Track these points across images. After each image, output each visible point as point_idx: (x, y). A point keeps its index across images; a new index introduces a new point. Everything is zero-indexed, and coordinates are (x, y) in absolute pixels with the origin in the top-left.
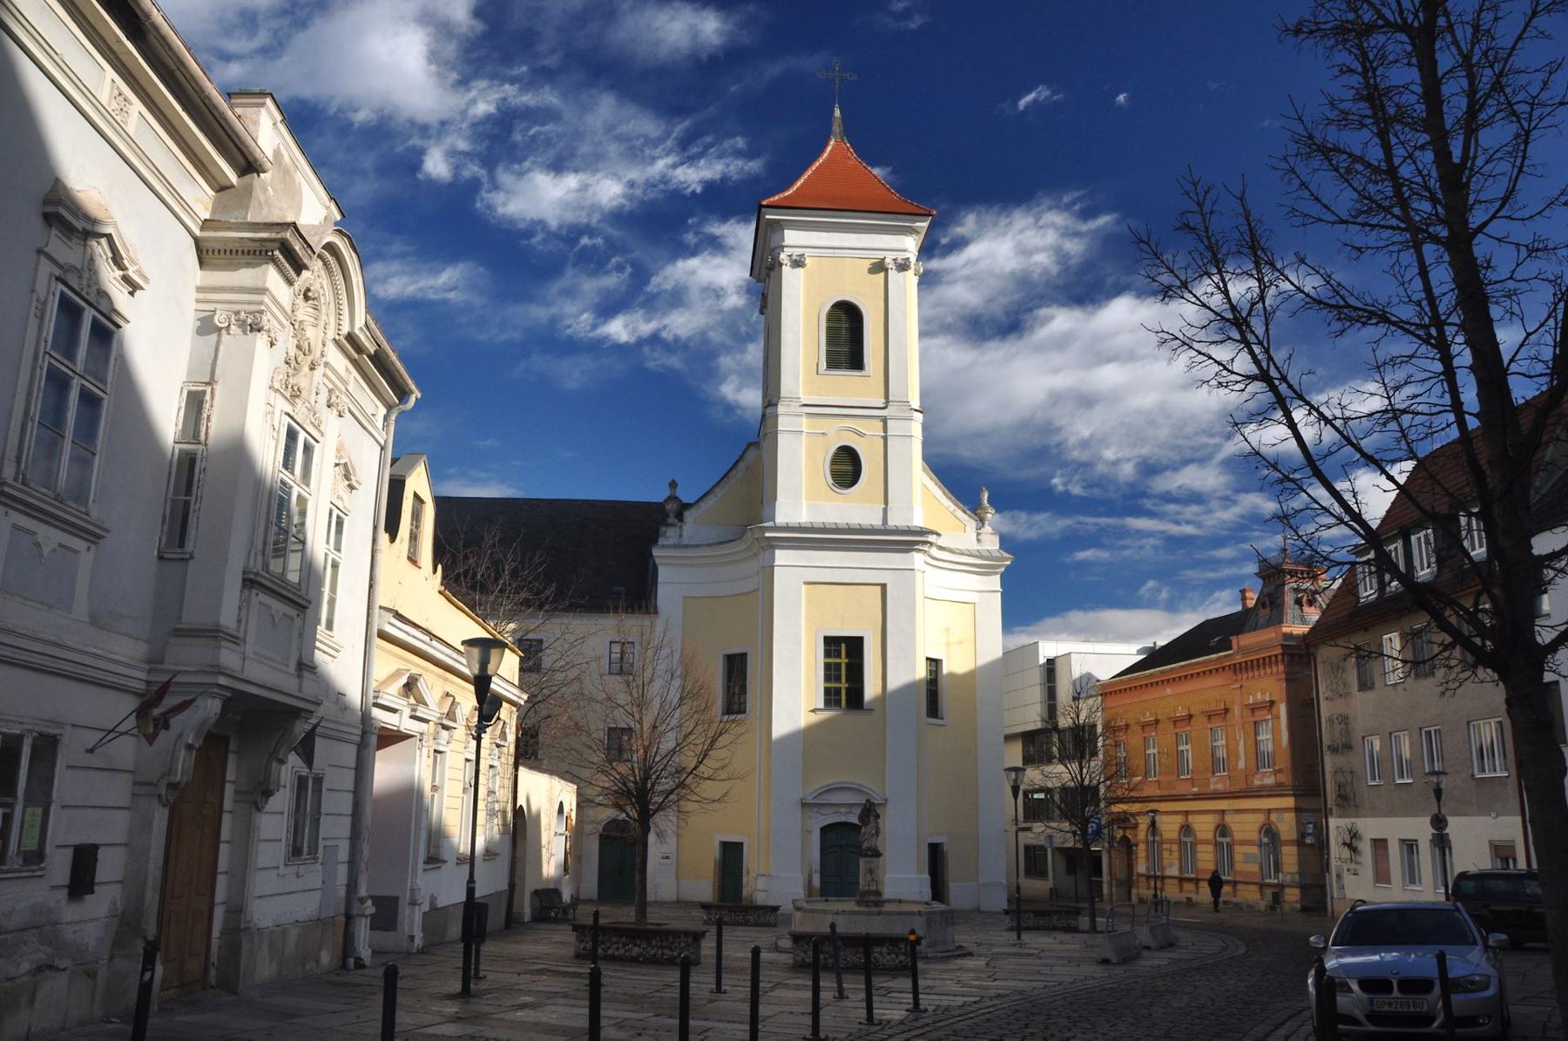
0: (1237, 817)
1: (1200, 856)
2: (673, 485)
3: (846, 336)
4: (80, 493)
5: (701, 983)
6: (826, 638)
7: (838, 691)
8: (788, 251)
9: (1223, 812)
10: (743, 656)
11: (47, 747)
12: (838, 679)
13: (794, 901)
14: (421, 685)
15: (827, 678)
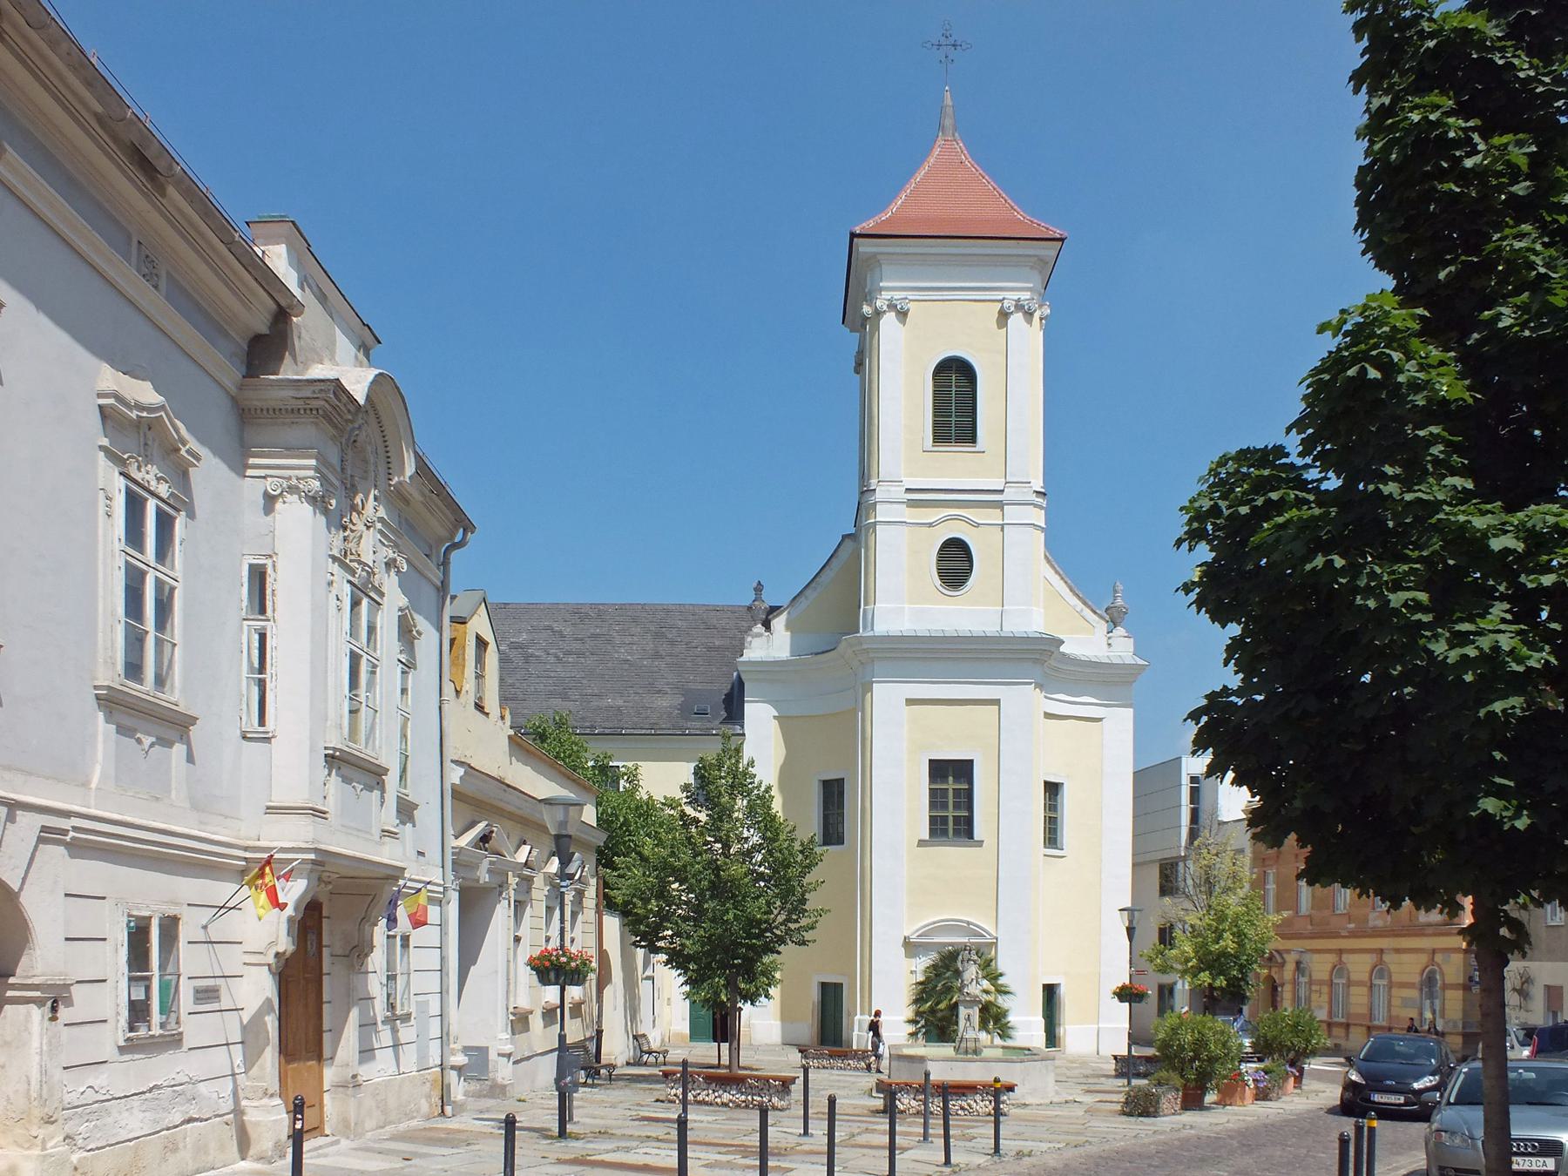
0: (1396, 957)
1: (1353, 1000)
2: (759, 588)
5: (783, 1130)
9: (1382, 951)
10: (840, 782)
11: (170, 925)
12: (945, 806)
15: (933, 805)
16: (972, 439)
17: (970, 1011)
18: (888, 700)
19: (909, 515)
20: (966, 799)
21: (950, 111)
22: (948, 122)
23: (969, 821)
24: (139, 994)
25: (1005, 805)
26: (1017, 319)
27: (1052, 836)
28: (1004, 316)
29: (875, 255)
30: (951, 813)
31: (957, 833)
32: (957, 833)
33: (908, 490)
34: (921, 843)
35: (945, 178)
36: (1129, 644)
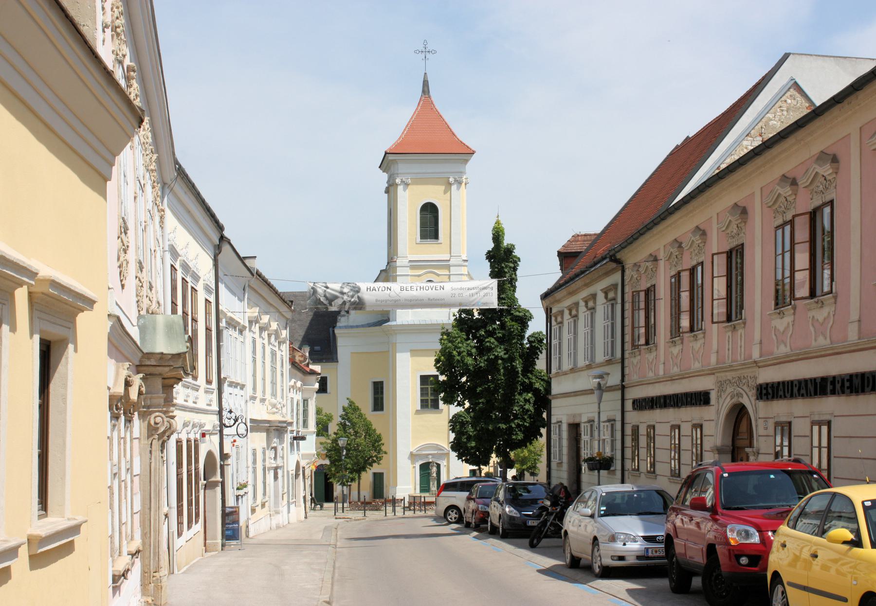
15: (422, 395)
16: (436, 237)
19: (410, 272)
24: (115, 470)
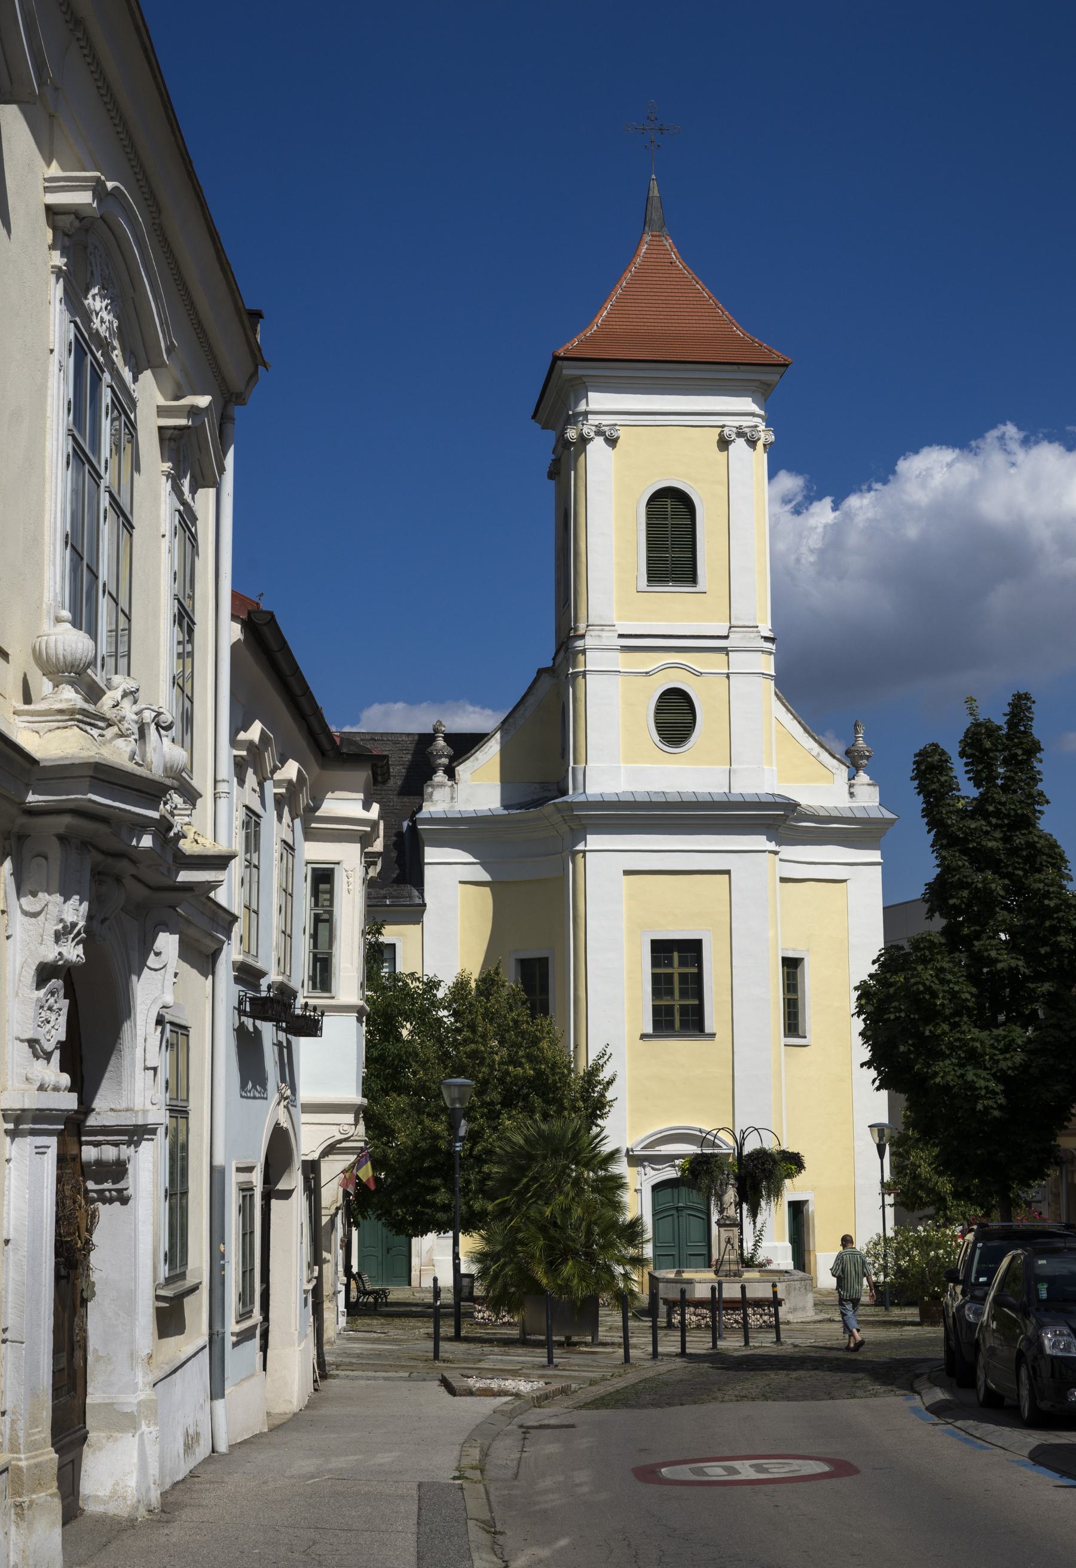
3: (672, 537)
4: (30, 1047)
6: (653, 942)
7: (670, 1009)
8: (593, 420)
12: (670, 992)
13: (1032, 719)
14: (30, 1076)
15: (656, 993)
17: (730, 1234)
18: (605, 865)
19: (623, 662)
20: (694, 985)
21: (656, 203)
22: (655, 215)
23: (699, 1010)
25: (739, 991)
26: (739, 446)
27: (793, 1024)
28: (724, 444)
29: (580, 377)
30: (677, 1002)
31: (685, 1025)
32: (685, 1025)
33: (621, 636)
34: (644, 1036)
35: (657, 279)
36: (875, 792)
